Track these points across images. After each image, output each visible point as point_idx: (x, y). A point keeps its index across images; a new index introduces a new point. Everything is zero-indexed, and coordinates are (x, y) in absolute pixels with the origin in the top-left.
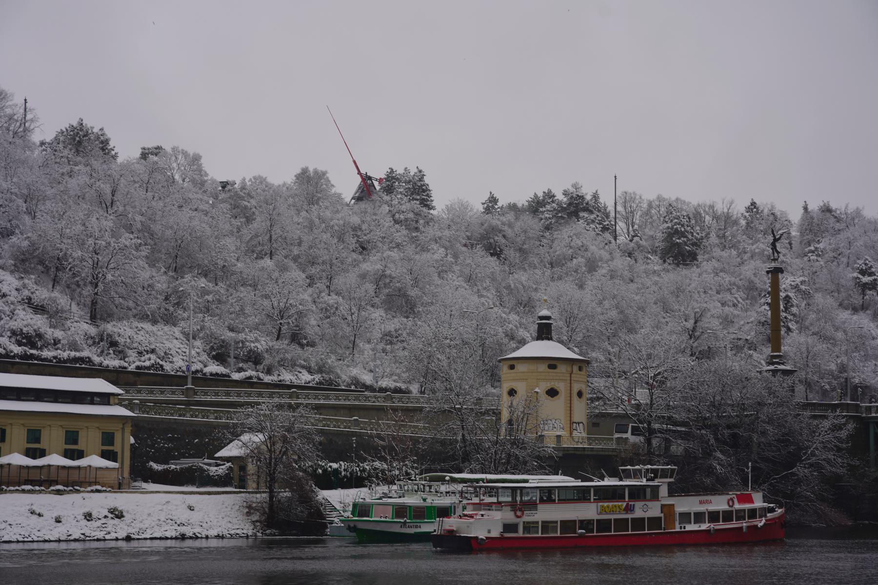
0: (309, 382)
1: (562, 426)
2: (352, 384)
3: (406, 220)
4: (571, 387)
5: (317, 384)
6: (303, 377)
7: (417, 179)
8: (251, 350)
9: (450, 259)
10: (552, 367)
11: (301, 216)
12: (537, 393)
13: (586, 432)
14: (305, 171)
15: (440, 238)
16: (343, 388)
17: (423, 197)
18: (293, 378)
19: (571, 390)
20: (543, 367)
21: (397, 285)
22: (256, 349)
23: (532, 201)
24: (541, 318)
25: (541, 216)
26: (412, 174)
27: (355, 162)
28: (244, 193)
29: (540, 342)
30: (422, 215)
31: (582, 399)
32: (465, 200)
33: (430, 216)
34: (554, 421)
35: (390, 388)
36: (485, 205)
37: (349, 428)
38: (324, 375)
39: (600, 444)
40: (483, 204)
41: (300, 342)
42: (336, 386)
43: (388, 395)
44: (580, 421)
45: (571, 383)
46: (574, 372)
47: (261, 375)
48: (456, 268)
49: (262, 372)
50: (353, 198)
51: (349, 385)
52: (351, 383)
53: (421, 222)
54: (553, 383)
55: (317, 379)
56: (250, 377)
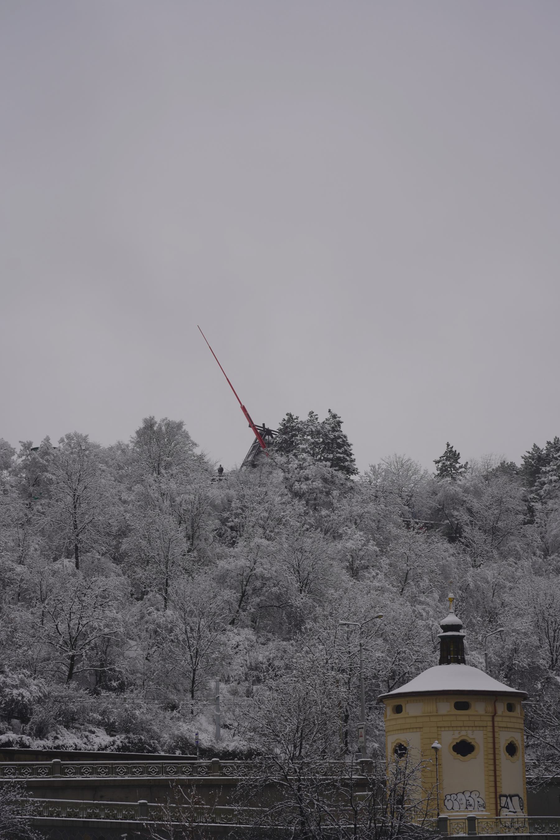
0: (106, 747)
1: (482, 802)
2: (176, 747)
3: (312, 491)
4: (494, 737)
5: (119, 749)
6: (97, 740)
7: (328, 427)
8: (13, 700)
9: (372, 547)
10: (462, 706)
11: (134, 491)
12: (436, 749)
13: (525, 809)
14: (149, 425)
15: (361, 516)
16: (163, 754)
17: (338, 455)
18: (80, 743)
19: (494, 743)
20: (446, 707)
21: (274, 589)
22: (20, 698)
23: (530, 457)
24: (446, 628)
25: (543, 479)
26: (321, 420)
27: (244, 409)
28: (47, 461)
29: (444, 667)
30: (337, 482)
31: (515, 757)
32: (406, 458)
33: (349, 484)
34: (468, 794)
35: (241, 752)
36: (440, 464)
37: (132, 818)
38: (131, 735)
39: (543, 829)
40: (437, 462)
41: (107, 685)
42: (149, 751)
43: (214, 762)
44: (512, 793)
45: (494, 732)
46: (499, 712)
47: (26, 739)
48: (384, 561)
49: (29, 735)
50: (243, 465)
51: (172, 750)
52: (176, 746)
53: (335, 493)
54: (463, 733)
55: (118, 743)
56: (9, 743)
